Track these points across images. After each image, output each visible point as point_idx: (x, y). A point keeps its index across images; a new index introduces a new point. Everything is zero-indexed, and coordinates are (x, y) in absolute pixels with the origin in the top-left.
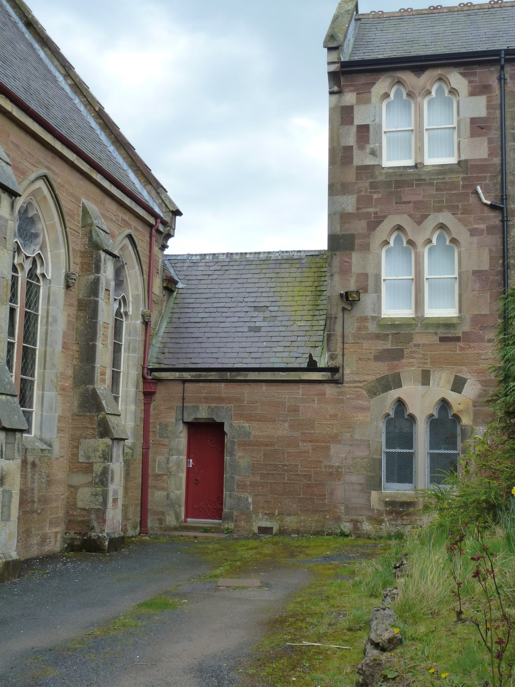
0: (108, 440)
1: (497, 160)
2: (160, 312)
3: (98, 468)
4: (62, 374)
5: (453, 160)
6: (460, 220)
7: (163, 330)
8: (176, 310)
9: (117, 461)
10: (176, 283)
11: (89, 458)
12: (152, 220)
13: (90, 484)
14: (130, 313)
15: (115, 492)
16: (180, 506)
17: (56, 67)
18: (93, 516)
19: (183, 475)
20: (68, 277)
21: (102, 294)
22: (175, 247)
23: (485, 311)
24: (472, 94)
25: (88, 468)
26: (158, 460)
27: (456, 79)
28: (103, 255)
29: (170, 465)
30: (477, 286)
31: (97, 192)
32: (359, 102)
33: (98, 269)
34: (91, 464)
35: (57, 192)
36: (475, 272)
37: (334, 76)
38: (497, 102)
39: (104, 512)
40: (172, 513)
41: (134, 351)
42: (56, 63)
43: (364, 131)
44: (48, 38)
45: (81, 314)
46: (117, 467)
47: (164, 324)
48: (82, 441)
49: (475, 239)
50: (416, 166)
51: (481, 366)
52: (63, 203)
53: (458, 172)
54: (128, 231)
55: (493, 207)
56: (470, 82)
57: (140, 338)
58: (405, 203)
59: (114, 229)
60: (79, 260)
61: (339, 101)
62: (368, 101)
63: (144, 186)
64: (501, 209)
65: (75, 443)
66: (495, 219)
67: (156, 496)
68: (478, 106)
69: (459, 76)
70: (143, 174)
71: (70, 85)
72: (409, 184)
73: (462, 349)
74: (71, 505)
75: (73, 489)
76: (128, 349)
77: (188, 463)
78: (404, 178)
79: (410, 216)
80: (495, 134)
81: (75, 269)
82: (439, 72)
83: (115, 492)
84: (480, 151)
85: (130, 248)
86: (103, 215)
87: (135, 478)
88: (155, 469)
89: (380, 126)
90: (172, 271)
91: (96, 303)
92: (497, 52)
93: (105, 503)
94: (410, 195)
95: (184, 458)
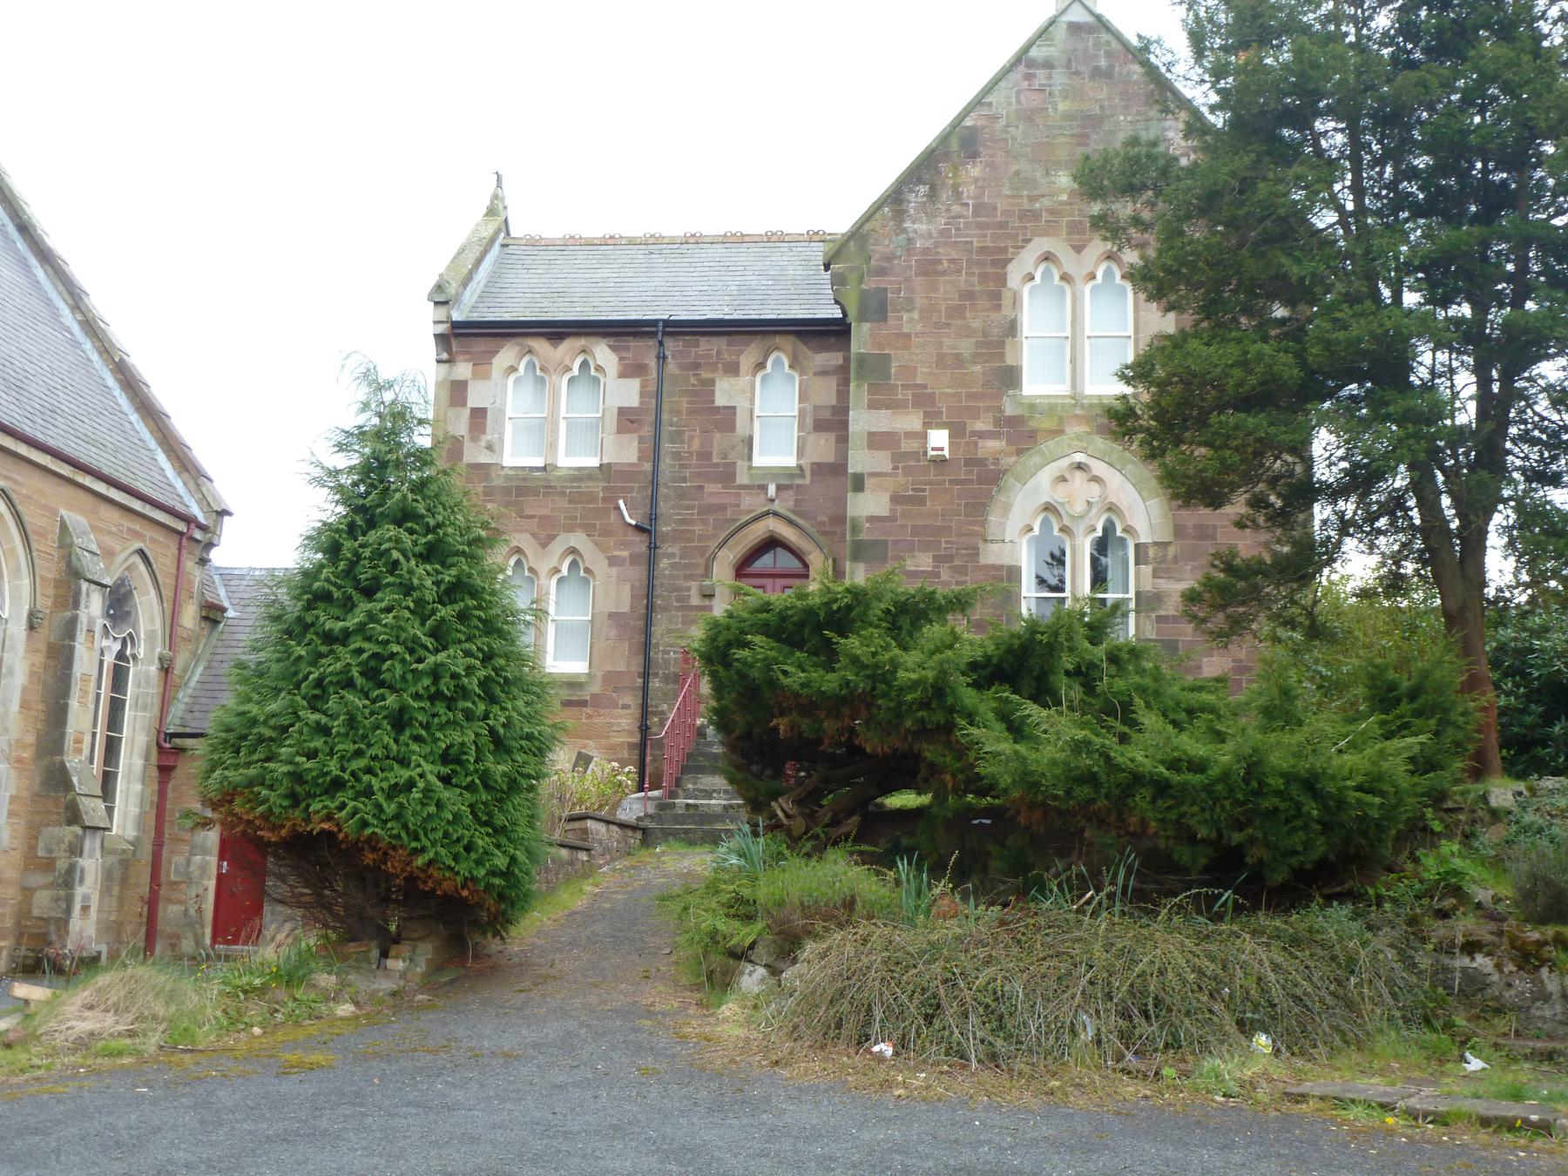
0: (78, 830)
1: (648, 466)
2: (194, 653)
3: (62, 864)
4: (17, 741)
5: (594, 462)
6: (596, 544)
7: (196, 678)
8: (219, 650)
9: (91, 856)
10: (224, 610)
11: (50, 851)
12: (181, 527)
13: (50, 886)
14: (141, 656)
15: (86, 898)
16: (203, 926)
17: (60, 293)
18: (52, 928)
19: (212, 884)
20: (32, 615)
21: (81, 636)
22: (217, 557)
23: (622, 667)
24: (622, 375)
25: (49, 865)
26: (174, 862)
27: (603, 354)
28: (84, 586)
29: (192, 868)
30: (613, 633)
31: (88, 498)
32: (476, 376)
33: (76, 605)
34: (53, 860)
35: (19, 508)
36: (611, 615)
37: (441, 339)
38: (652, 388)
39: (67, 923)
40: (190, 936)
41: (145, 709)
42: (61, 288)
43: (479, 415)
44: (50, 250)
45: (51, 662)
46: (91, 864)
47: (200, 670)
48: (44, 829)
49: (614, 571)
50: (544, 469)
51: (613, 740)
52: (27, 519)
53: (598, 480)
54: (137, 545)
55: (638, 528)
56: (621, 359)
57: (154, 690)
58: (528, 517)
59: (106, 545)
60: (51, 591)
61: (449, 373)
62: (487, 376)
63: (179, 474)
64: (648, 531)
65: (34, 833)
66: (640, 544)
67: (170, 912)
68: (628, 393)
69: (607, 350)
70: (178, 457)
71: (79, 322)
72: (534, 492)
73: (589, 716)
74: (24, 913)
75: (28, 892)
76: (135, 706)
77: (220, 867)
78: (528, 484)
79: (533, 535)
80: (647, 431)
81: (45, 604)
82: (582, 342)
83: (86, 898)
84: (626, 452)
85: (142, 567)
86: (93, 528)
87: (138, 886)
88: (171, 874)
89: (502, 411)
90: (222, 592)
91: (71, 649)
92: (654, 323)
93: (68, 911)
94: (534, 507)
95: (213, 860)
